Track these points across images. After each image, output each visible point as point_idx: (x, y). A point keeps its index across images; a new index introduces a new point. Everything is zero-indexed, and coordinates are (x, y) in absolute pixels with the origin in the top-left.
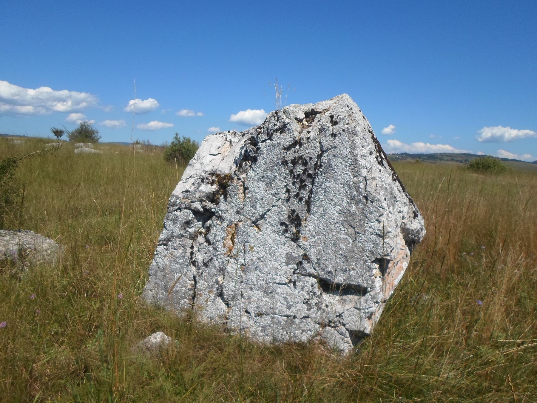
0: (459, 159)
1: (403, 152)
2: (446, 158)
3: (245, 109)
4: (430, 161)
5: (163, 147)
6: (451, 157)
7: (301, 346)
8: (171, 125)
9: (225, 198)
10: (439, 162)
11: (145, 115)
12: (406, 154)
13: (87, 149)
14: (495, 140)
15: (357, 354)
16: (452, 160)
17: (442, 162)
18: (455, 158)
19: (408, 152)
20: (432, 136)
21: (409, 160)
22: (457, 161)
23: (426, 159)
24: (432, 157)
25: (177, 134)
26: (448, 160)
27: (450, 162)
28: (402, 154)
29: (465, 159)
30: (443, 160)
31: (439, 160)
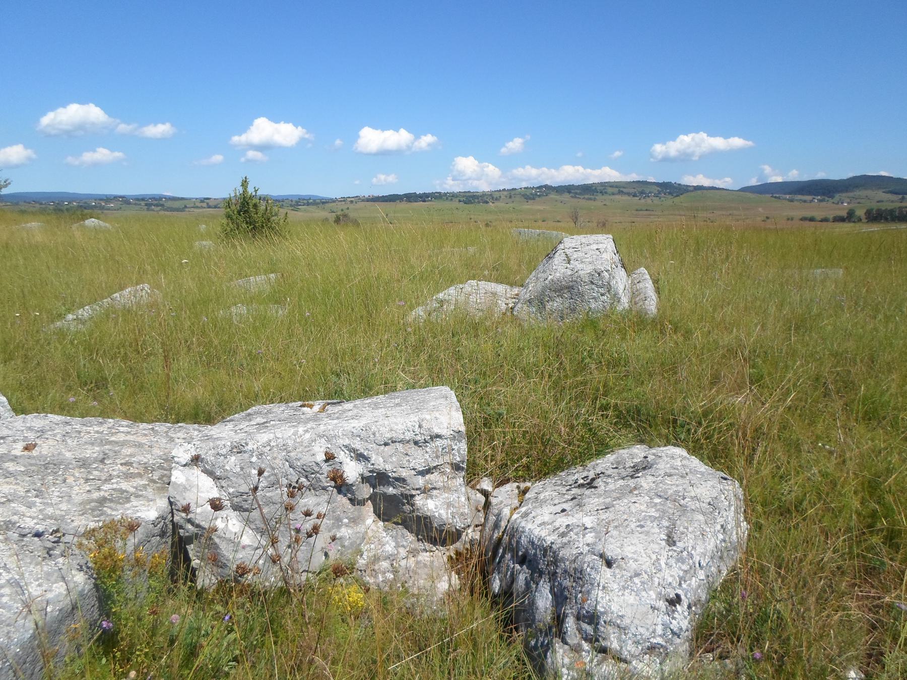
0: (632, 191)
2: (610, 190)
3: (156, 123)
4: (586, 196)
5: (228, 203)
6: (619, 188)
7: (642, 442)
10: (599, 197)
11: (81, 137)
12: (546, 186)
13: (285, 433)
16: (621, 192)
17: (605, 197)
18: (624, 190)
19: (548, 183)
20: (338, 142)
21: (553, 196)
22: (629, 194)
23: (580, 194)
25: (245, 183)
26: (613, 194)
27: (618, 197)
28: (540, 187)
29: (640, 190)
30: (606, 193)
31: (600, 195)
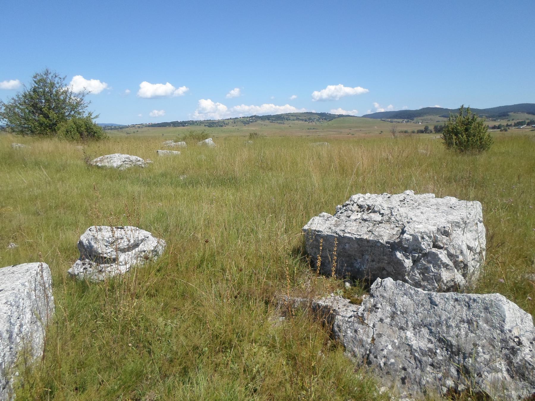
0: (304, 118)
1: (253, 115)
2: (291, 118)
4: (279, 122)
6: (297, 117)
8: (359, 90)
9: (27, 352)
12: (255, 116)
14: (331, 99)
15: (32, 132)
16: (298, 119)
18: (300, 118)
20: (128, 91)
22: (302, 120)
23: (275, 120)
24: (279, 118)
27: (296, 122)
28: (252, 117)
29: (309, 117)
30: (289, 119)
